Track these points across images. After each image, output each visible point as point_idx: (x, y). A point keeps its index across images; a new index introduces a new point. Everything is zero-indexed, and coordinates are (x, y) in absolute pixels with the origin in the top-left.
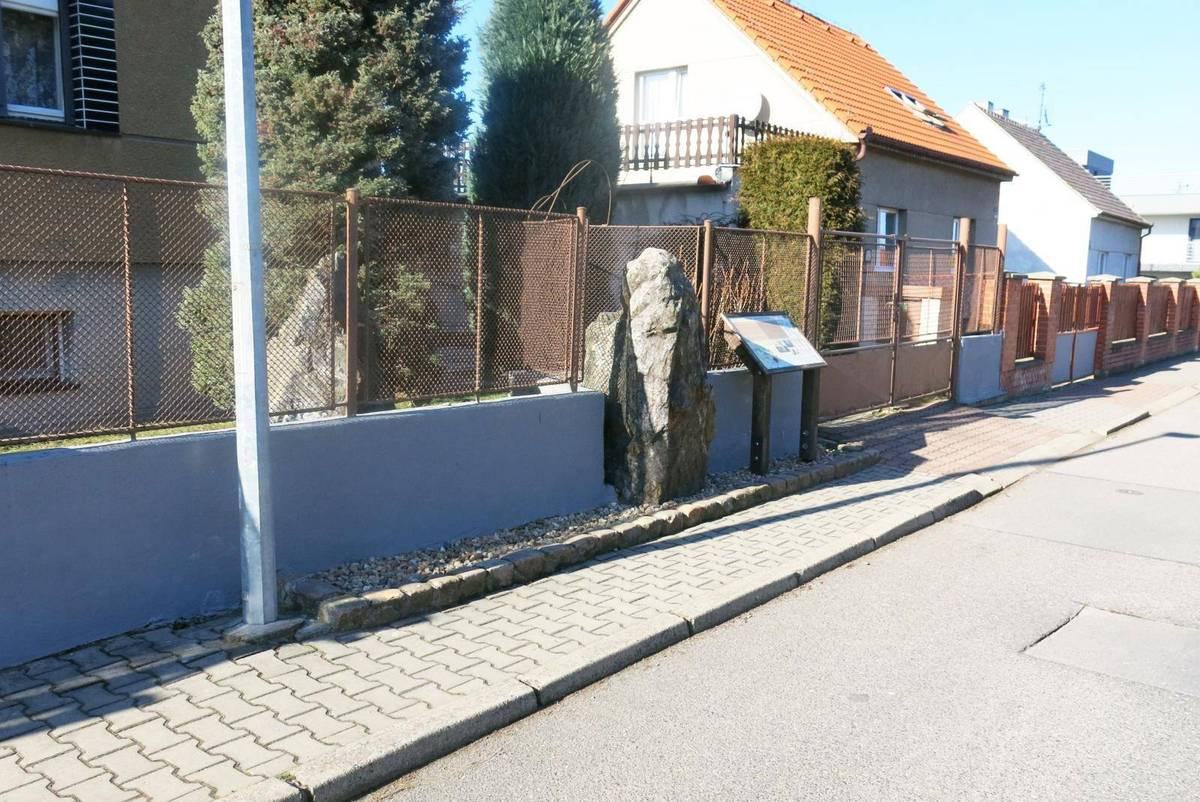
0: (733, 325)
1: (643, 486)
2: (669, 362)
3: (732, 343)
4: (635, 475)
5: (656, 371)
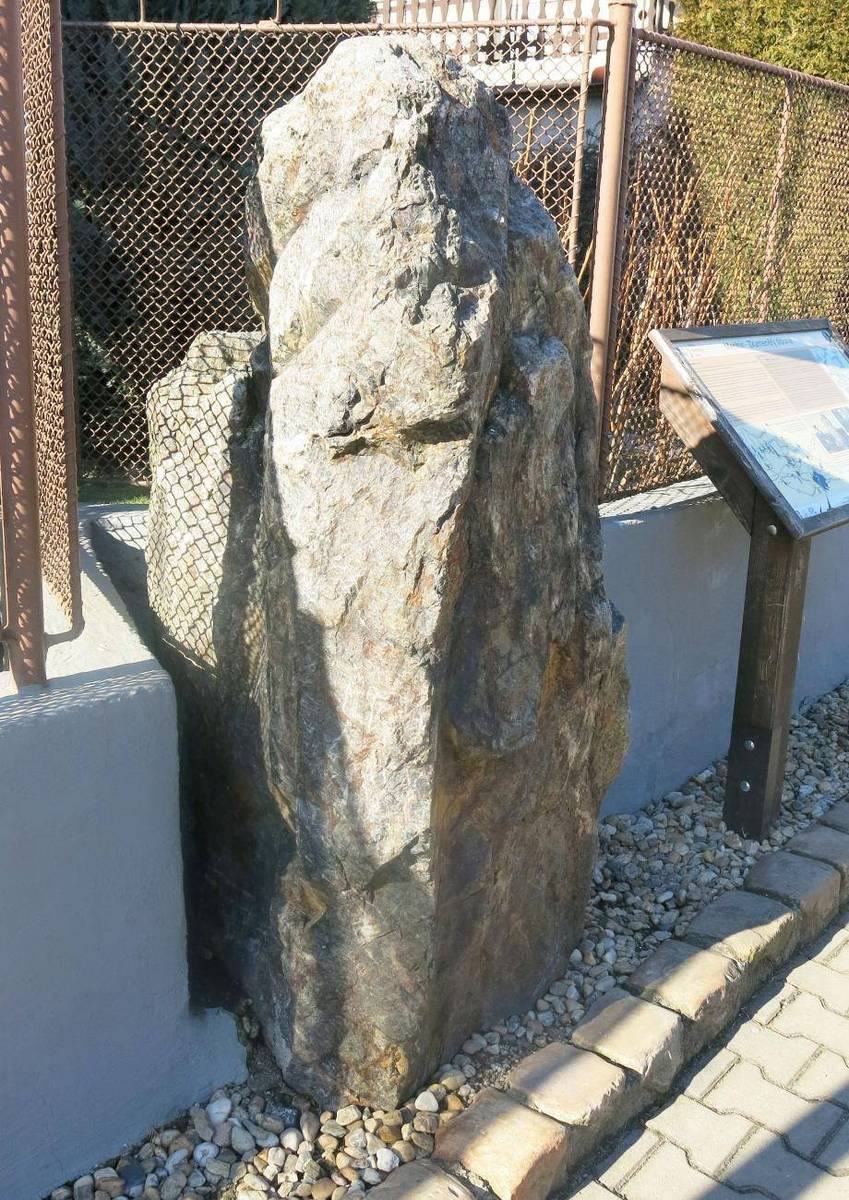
0: (692, 371)
1: (337, 1041)
2: (434, 572)
3: (687, 424)
4: (305, 997)
5: (374, 607)
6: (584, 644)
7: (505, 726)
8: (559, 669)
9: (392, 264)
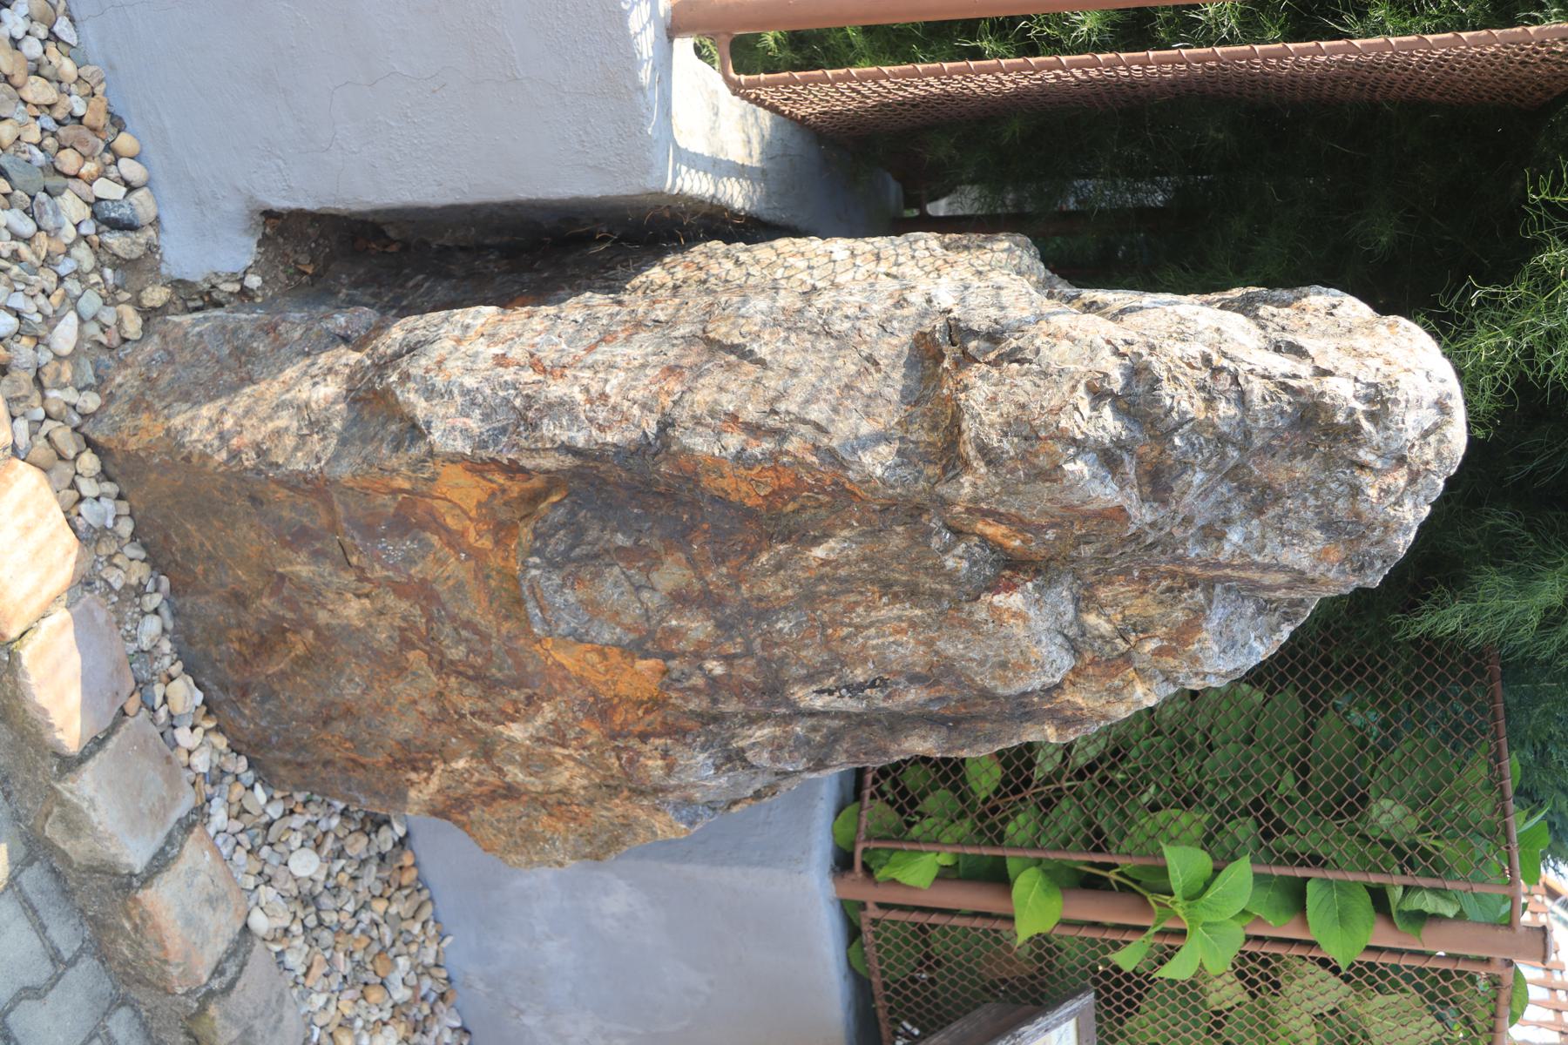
6: (659, 736)
7: (556, 579)
8: (628, 699)
9: (1164, 359)
